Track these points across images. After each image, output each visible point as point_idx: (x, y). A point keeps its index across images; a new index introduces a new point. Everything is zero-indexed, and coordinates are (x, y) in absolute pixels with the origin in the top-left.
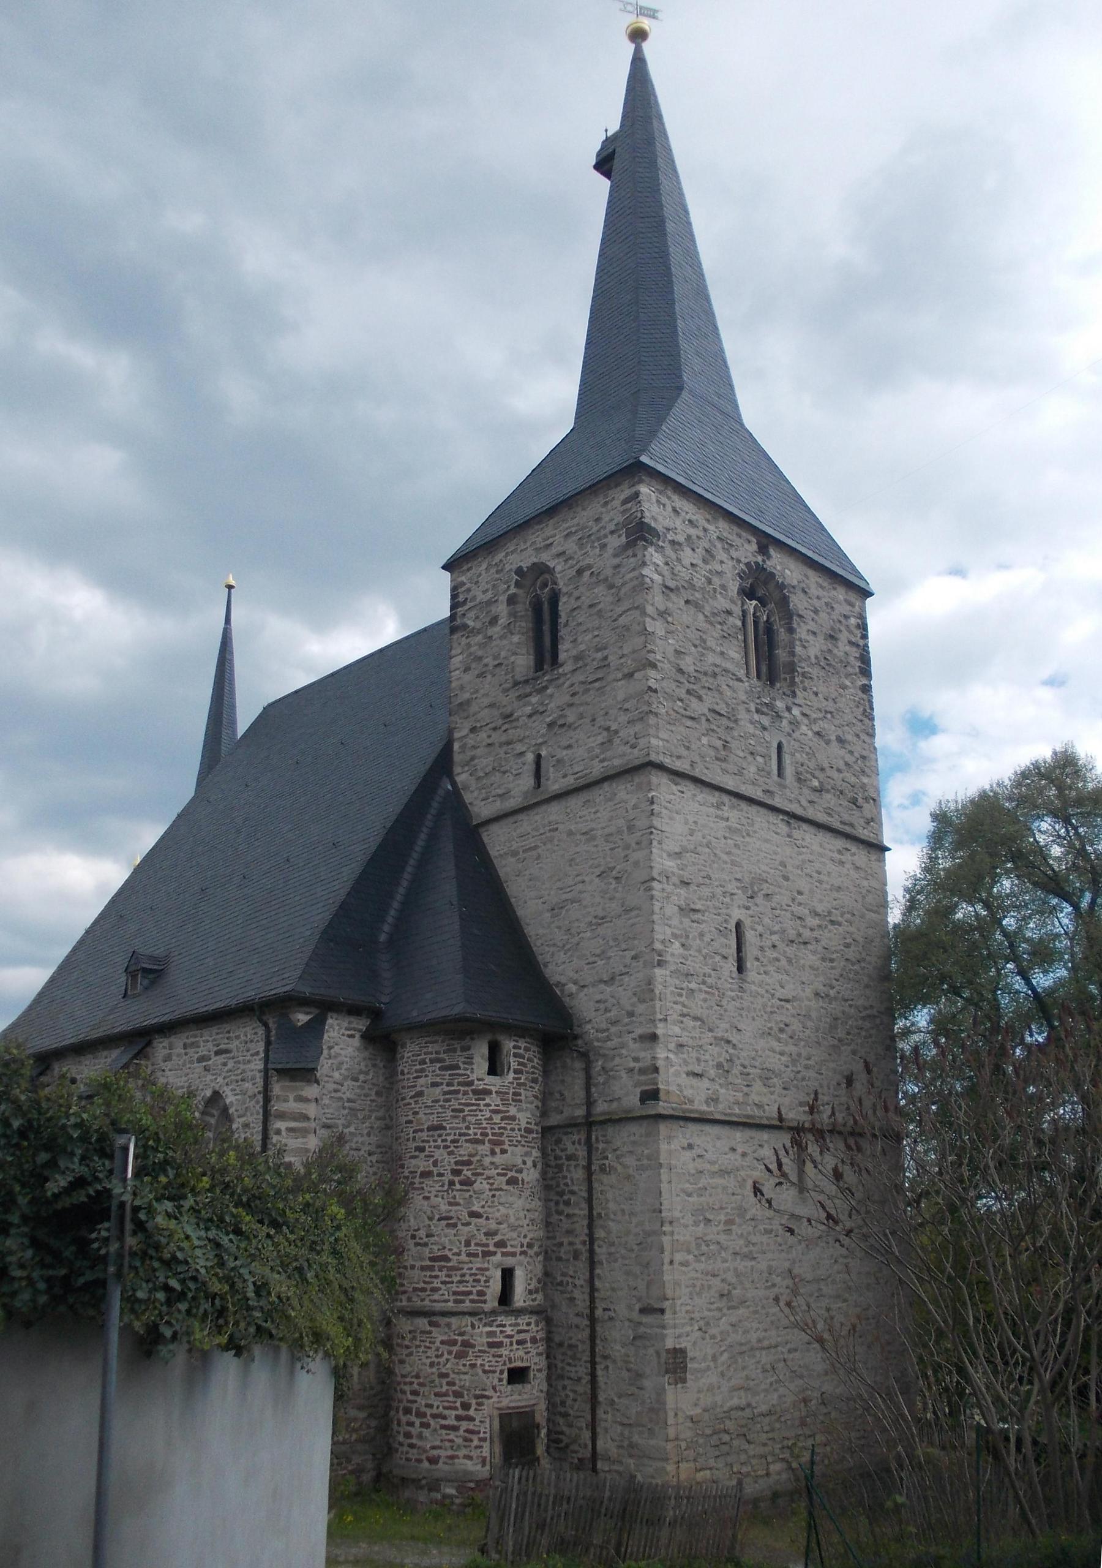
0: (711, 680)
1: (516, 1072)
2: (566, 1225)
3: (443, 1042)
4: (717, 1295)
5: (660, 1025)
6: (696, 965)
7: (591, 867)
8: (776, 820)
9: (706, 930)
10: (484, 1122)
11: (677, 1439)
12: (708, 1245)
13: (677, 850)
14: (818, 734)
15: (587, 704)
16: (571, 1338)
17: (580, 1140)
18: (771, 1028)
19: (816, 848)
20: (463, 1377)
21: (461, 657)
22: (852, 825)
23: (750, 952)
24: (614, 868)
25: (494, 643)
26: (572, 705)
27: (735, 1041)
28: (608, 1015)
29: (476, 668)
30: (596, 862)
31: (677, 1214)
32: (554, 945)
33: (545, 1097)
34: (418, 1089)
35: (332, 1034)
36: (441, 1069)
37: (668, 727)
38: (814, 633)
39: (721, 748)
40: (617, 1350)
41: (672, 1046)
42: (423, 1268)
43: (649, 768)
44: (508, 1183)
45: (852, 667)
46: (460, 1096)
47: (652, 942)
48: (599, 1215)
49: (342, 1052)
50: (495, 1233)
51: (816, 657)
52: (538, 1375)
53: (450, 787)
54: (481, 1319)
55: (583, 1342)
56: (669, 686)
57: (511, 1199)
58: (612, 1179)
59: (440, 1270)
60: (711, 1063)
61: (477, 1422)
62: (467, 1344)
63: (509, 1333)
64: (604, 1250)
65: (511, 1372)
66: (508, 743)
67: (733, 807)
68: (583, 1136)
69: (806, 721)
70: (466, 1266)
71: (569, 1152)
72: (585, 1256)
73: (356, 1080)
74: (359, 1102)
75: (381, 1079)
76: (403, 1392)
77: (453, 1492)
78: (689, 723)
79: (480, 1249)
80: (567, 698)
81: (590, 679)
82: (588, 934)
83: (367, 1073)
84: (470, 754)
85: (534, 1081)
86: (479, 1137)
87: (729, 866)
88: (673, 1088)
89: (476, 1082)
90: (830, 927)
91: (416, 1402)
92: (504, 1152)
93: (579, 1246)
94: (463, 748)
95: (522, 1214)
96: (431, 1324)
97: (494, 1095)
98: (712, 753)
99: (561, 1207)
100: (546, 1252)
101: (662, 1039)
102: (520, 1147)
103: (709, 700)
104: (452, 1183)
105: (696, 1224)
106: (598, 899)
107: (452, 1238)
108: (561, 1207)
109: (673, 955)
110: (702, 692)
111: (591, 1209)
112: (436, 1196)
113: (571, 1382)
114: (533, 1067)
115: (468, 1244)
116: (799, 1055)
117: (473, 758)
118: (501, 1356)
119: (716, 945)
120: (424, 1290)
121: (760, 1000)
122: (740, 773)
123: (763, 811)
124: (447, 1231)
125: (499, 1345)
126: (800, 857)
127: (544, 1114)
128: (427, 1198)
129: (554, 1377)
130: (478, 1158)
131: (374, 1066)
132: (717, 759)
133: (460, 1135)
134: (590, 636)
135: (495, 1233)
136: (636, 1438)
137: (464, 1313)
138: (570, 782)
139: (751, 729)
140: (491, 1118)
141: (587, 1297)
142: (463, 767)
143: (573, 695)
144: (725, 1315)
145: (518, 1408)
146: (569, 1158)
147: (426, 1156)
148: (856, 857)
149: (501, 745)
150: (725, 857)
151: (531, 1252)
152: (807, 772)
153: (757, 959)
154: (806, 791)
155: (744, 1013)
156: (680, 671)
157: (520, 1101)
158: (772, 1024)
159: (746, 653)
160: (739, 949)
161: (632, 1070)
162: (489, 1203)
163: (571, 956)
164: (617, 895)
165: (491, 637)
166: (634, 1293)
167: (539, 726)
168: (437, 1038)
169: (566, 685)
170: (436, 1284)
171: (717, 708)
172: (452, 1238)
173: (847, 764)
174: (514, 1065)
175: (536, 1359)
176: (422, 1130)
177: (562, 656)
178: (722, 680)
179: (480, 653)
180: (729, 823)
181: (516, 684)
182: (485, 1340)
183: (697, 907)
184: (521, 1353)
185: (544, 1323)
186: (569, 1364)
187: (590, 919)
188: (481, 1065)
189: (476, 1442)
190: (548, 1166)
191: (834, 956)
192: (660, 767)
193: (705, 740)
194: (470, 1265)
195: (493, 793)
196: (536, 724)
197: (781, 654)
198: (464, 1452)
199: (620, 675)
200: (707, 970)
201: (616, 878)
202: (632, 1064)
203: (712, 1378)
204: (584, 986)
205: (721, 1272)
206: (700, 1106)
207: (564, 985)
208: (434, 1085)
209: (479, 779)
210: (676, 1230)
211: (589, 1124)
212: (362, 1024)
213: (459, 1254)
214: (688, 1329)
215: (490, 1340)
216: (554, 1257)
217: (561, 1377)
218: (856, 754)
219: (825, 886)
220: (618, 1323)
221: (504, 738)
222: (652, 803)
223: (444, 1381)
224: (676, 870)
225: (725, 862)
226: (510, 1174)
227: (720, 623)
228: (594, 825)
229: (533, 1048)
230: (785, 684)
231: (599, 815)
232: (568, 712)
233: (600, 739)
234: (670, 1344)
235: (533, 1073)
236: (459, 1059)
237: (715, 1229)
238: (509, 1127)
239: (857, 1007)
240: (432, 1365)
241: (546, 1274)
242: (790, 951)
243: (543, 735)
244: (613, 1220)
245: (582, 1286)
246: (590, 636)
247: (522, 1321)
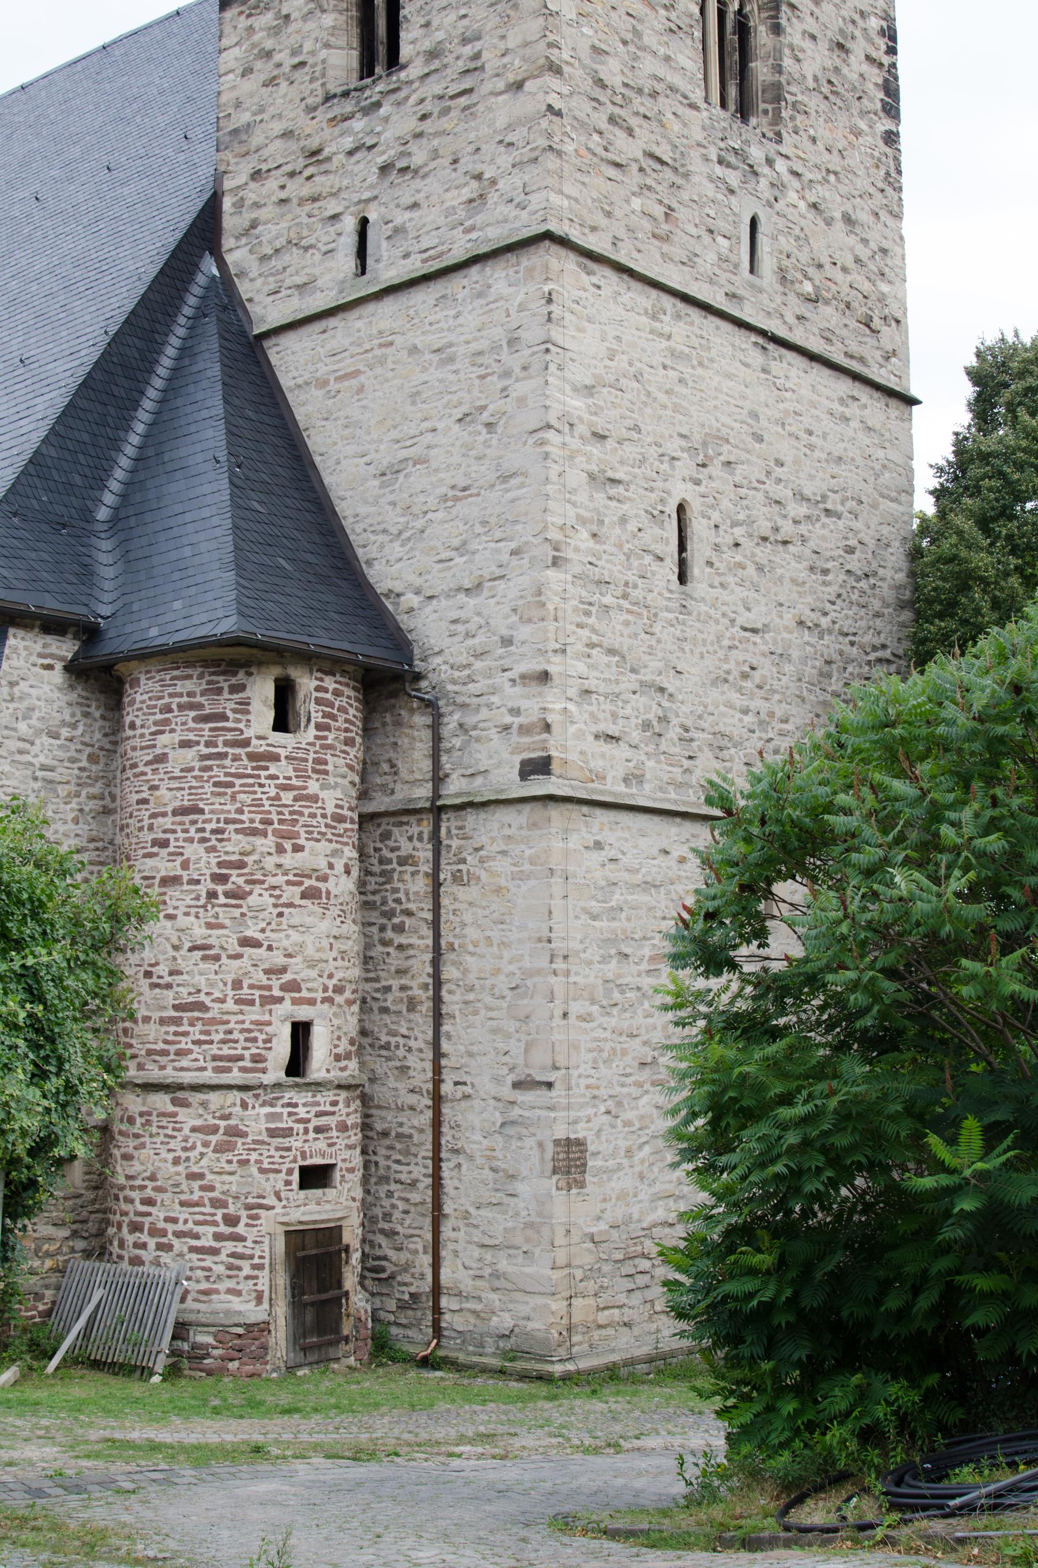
0: (648, 102)
1: (319, 727)
2: (396, 960)
3: (201, 676)
4: (636, 1064)
5: (557, 659)
6: (611, 568)
7: (445, 406)
8: (747, 340)
9: (631, 513)
10: (267, 803)
11: (569, 1265)
12: (623, 992)
13: (588, 382)
14: (814, 206)
15: (444, 133)
16: (401, 1125)
17: (420, 834)
18: (728, 672)
19: (805, 392)
20: (226, 1178)
21: (237, 49)
22: (862, 360)
23: (698, 552)
24: (484, 408)
25: (293, 27)
26: (419, 135)
27: (671, 689)
28: (470, 642)
29: (263, 70)
30: (455, 398)
31: (575, 945)
32: (385, 531)
33: (366, 769)
34: (158, 751)
35: (15, 663)
36: (197, 719)
37: (578, 175)
38: (813, 37)
39: (661, 217)
40: (475, 1142)
41: (572, 692)
42: (163, 1021)
43: (547, 243)
44: (304, 896)
45: (871, 100)
46: (227, 762)
47: (545, 528)
48: (452, 948)
49: (34, 692)
50: (284, 970)
51: (816, 79)
52: (349, 1176)
53: (215, 271)
54: (257, 1096)
55: (421, 1131)
56: (581, 107)
57: (309, 920)
58: (472, 893)
59: (191, 1024)
60: (634, 721)
61: (249, 1243)
62: (235, 1132)
63: (303, 1115)
64: (457, 997)
65: (303, 1170)
66: (315, 199)
67: (678, 317)
68: (426, 828)
69: (796, 184)
70: (233, 1018)
71: (403, 853)
72: (426, 1007)
73: (56, 736)
74: (60, 770)
75: (98, 736)
76: (130, 1201)
77: (209, 1340)
78: (612, 172)
79: (257, 993)
80: (412, 124)
81: (451, 92)
82: (440, 515)
83: (74, 726)
84: (248, 216)
85: (349, 742)
86: (257, 825)
87: (669, 412)
88: (573, 756)
89: (254, 742)
90: (824, 519)
91: (149, 1214)
92: (298, 849)
93: (417, 992)
94: (239, 204)
95: (325, 943)
96: (175, 1102)
97: (284, 762)
98: (646, 225)
99: (389, 934)
100: (364, 1001)
101: (556, 680)
102: (324, 843)
103: (645, 137)
104: (212, 895)
105: (605, 959)
106: (456, 459)
107: (212, 976)
108: (389, 934)
109: (577, 550)
110: (634, 122)
111: (437, 936)
112: (187, 914)
113: (399, 1186)
114: (347, 721)
115: (237, 984)
116: (771, 714)
117: (254, 224)
118: (289, 1149)
119: (646, 537)
120: (164, 1053)
121: (713, 628)
122: (689, 262)
123: (726, 326)
124: (203, 966)
125: (288, 1133)
126: (781, 406)
127: (364, 795)
128: (170, 917)
129: (373, 1180)
130: (255, 857)
131: (86, 715)
132: (654, 236)
133: (227, 821)
134: (453, 16)
135: (284, 970)
136: (503, 1265)
137: (229, 1087)
138: (415, 267)
139: (710, 190)
140: (278, 798)
141: (429, 1066)
142: (237, 238)
143: (424, 117)
144: (647, 1092)
145: (315, 1222)
146: (403, 861)
147: (170, 854)
148: (867, 412)
149: (302, 201)
150: (662, 397)
151: (339, 999)
152: (795, 268)
153: (710, 564)
154: (792, 299)
155: (687, 647)
156: (600, 83)
157: (326, 773)
158: (731, 666)
159: (705, 62)
160: (682, 547)
161: (507, 728)
162: (273, 926)
163: (412, 549)
164: (488, 451)
165: (287, 17)
166: (506, 1059)
167: (366, 167)
168: (190, 671)
169: (412, 100)
170: (185, 1043)
171: (658, 152)
172: (212, 976)
173: (858, 261)
174: (317, 717)
175: (346, 1154)
176: (164, 815)
177: (406, 51)
178: (666, 104)
179: (268, 45)
180: (672, 343)
181: (328, 98)
182: (263, 1125)
183: (617, 476)
184: (321, 1145)
185: (358, 1102)
186: (398, 1162)
187: (443, 490)
188: (263, 715)
189: (247, 1271)
190: (368, 873)
191: (829, 565)
192: (564, 242)
193: (636, 203)
194: (240, 1017)
195: (288, 282)
196: (362, 166)
197: (761, 71)
198: (231, 1284)
199: (501, 85)
200: (631, 578)
201: (489, 425)
202: (508, 719)
203: (624, 1181)
204: (431, 598)
205: (643, 1031)
206: (614, 789)
207: (398, 595)
208: (185, 744)
209: (264, 258)
210: (574, 968)
211: (437, 811)
212: (66, 648)
213: (223, 1001)
214: (590, 1111)
215: (273, 1126)
216: (375, 1006)
217: (385, 1179)
218: (873, 245)
219: (817, 454)
220: (476, 1103)
221: (307, 190)
222: (550, 301)
223: (196, 1185)
224: (586, 416)
225: (664, 407)
226: (308, 882)
227: (665, 7)
228: (452, 337)
229: (348, 692)
230: (764, 120)
231: (461, 320)
232: (413, 147)
233: (466, 193)
234: (561, 1132)
235: (346, 730)
236: (227, 703)
237: (634, 969)
238: (306, 811)
239: (862, 647)
240: (176, 1161)
241: (363, 1033)
242: (762, 554)
243: (372, 187)
244: (472, 954)
245: (421, 1050)
246: (453, 16)
247: (325, 1099)
